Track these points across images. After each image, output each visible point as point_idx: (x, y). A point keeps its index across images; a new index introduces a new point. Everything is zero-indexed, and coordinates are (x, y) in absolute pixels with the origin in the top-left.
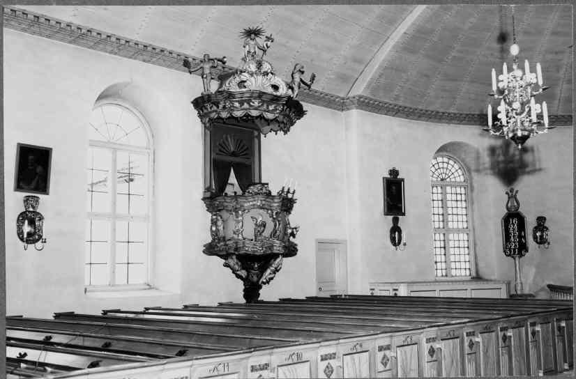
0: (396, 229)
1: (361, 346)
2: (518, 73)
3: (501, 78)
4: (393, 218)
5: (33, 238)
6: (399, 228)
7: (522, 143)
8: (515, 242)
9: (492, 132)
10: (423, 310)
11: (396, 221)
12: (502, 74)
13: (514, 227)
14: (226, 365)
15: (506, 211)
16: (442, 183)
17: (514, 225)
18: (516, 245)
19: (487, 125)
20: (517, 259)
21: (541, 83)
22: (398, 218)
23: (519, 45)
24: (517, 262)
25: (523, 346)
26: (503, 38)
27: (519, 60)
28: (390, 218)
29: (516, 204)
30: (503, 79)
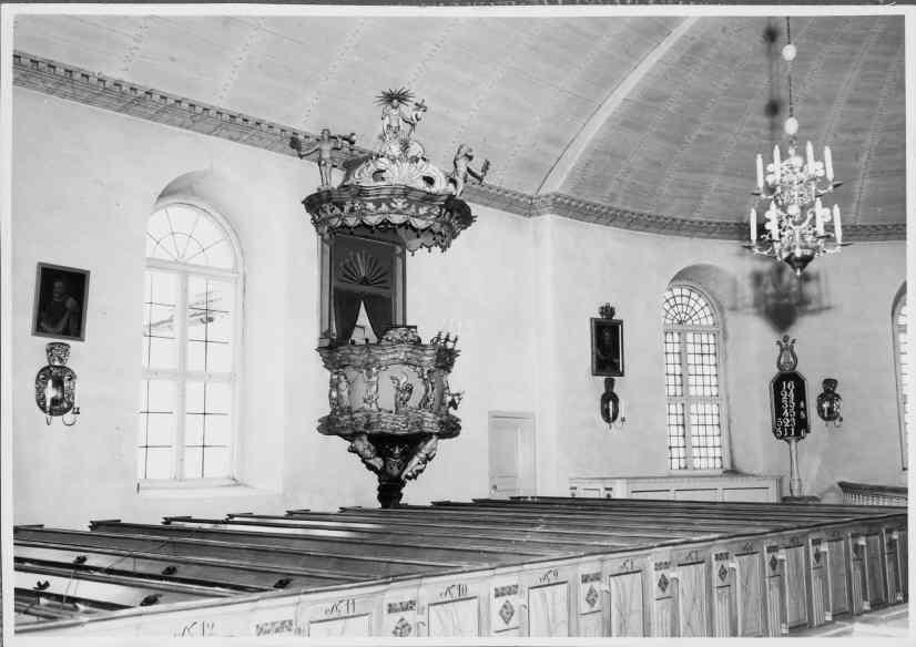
0: (609, 397)
2: (797, 161)
8: (789, 418)
9: (756, 251)
12: (772, 161)
13: (789, 395)
14: (351, 603)
17: (788, 391)
29: (791, 359)
30: (776, 171)
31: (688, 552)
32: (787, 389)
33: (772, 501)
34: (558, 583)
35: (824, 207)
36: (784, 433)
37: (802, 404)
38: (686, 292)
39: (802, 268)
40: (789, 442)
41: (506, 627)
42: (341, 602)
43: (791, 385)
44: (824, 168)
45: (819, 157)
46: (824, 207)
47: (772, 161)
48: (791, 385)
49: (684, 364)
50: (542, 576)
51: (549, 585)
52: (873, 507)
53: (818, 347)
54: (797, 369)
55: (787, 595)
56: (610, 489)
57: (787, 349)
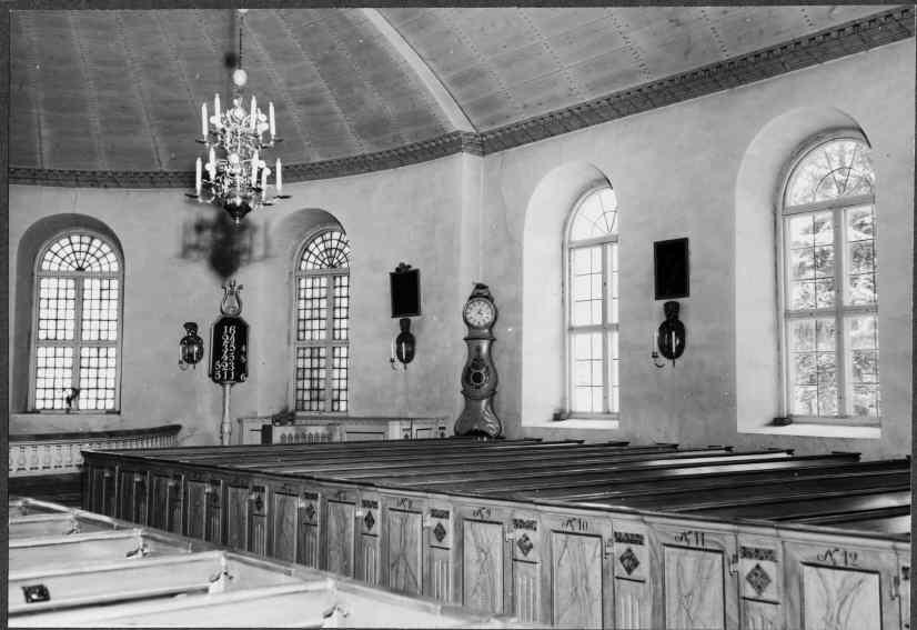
0: (672, 326)
1: (489, 512)
2: (239, 113)
3: (213, 120)
4: (666, 305)
5: (191, 327)
6: (681, 325)
7: (242, 217)
8: (228, 361)
9: (200, 200)
10: (301, 463)
11: (405, 326)
12: (214, 114)
13: (229, 340)
14: (700, 536)
15: (219, 313)
16: (80, 273)
17: (230, 335)
18: (230, 366)
19: (196, 191)
20: (228, 387)
21: (273, 132)
22: (409, 321)
23: (248, 74)
24: (227, 392)
25: (244, 518)
26: (231, 62)
27: (245, 92)
28: (397, 320)
29: (236, 304)
30: (213, 117)
31: (400, 497)
32: (230, 335)
33: (255, 443)
34: (491, 522)
35: (260, 158)
36: (223, 375)
37: (244, 348)
38: (66, 241)
39: (242, 217)
40: (223, 385)
41: (626, 575)
42: (837, 550)
43: (232, 329)
44: (268, 121)
45: (265, 110)
46: (260, 158)
47: (214, 114)
48: (232, 329)
49: (330, 297)
50: (476, 509)
51: (480, 521)
52: (137, 450)
53: (202, 296)
54: (242, 315)
55: (499, 559)
56: (444, 428)
57: (232, 293)
